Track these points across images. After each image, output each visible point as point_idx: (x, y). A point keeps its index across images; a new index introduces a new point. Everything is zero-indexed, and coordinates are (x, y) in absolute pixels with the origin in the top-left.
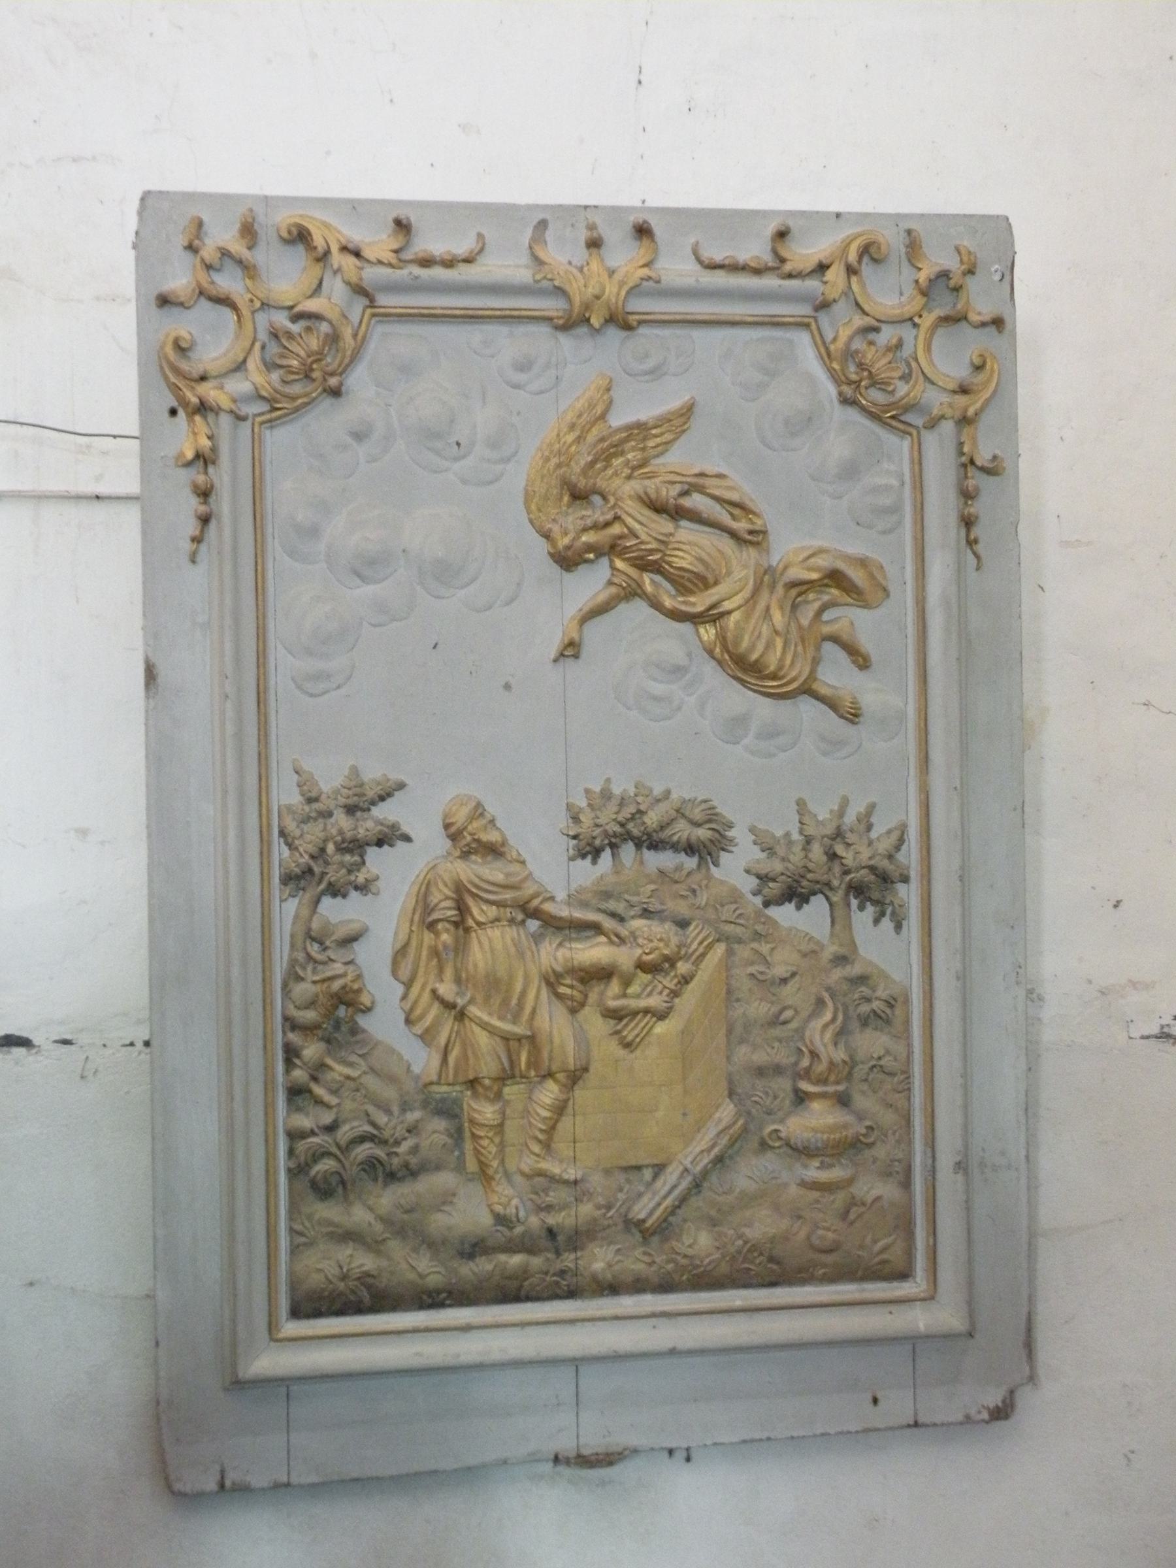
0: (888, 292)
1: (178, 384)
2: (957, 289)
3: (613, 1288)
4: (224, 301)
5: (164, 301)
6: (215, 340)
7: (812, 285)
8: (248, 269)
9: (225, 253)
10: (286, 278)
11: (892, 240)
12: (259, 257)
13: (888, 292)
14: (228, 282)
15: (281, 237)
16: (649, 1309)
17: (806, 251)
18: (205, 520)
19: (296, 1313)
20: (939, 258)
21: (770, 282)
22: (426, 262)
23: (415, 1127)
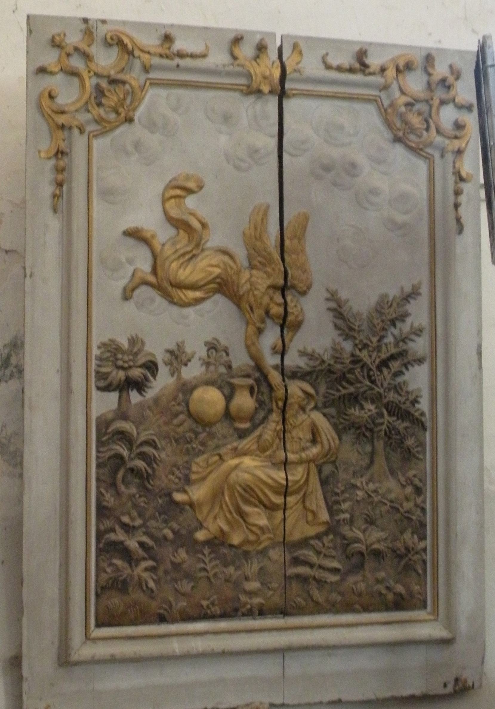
0: (415, 83)
1: (47, 109)
2: (449, 87)
3: (262, 613)
4: (74, 74)
5: (42, 71)
6: (68, 94)
7: (377, 79)
8: (87, 57)
9: (76, 49)
10: (106, 60)
11: (418, 60)
12: (93, 50)
13: (415, 83)
14: (77, 63)
15: (106, 39)
16: (383, 620)
17: (374, 61)
18: (60, 185)
19: (99, 625)
20: (441, 70)
21: (358, 77)
22: (181, 55)
23: (126, 120)
